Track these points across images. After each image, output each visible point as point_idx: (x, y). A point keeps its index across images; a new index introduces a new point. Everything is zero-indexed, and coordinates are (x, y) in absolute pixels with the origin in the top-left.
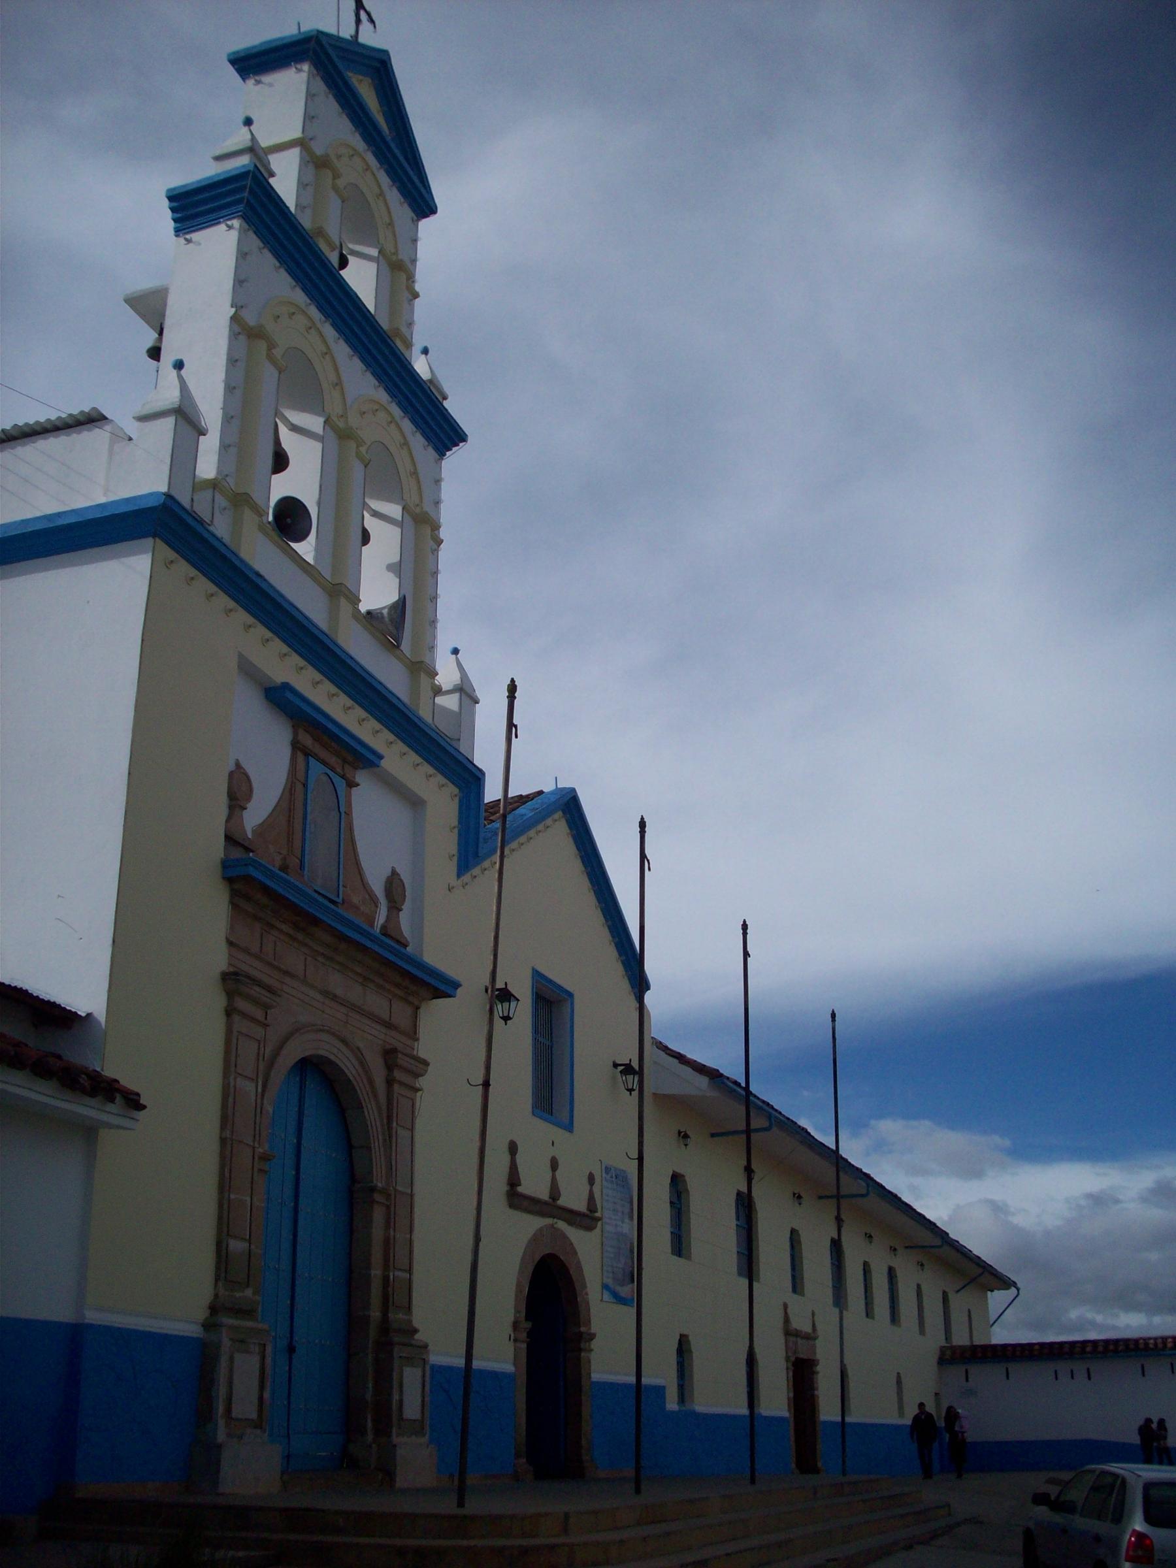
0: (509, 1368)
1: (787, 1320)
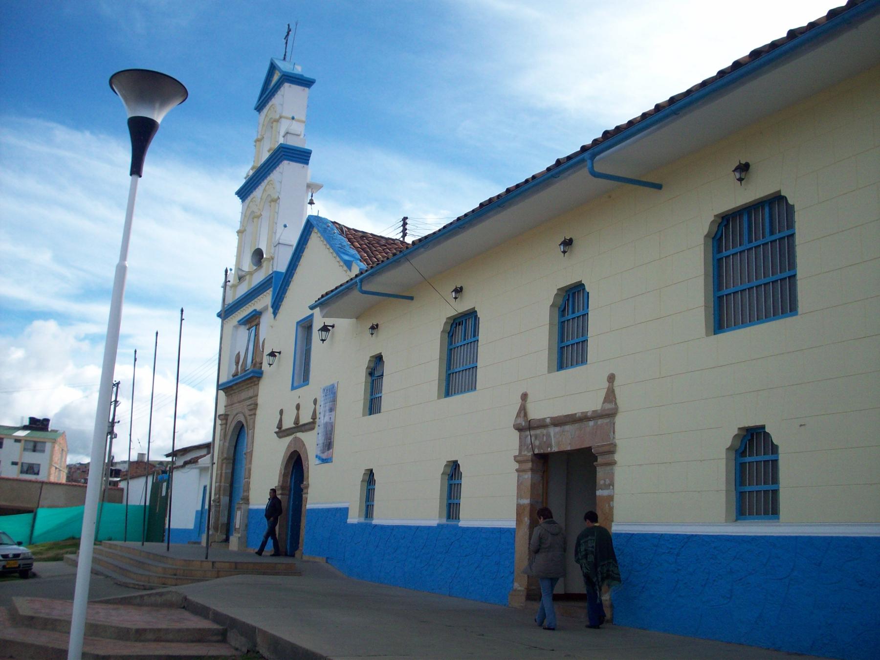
0: (510, 523)
1: (523, 411)
